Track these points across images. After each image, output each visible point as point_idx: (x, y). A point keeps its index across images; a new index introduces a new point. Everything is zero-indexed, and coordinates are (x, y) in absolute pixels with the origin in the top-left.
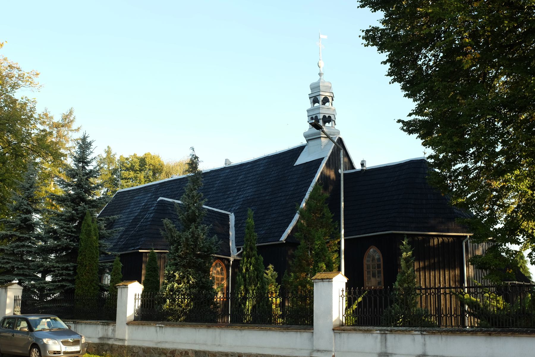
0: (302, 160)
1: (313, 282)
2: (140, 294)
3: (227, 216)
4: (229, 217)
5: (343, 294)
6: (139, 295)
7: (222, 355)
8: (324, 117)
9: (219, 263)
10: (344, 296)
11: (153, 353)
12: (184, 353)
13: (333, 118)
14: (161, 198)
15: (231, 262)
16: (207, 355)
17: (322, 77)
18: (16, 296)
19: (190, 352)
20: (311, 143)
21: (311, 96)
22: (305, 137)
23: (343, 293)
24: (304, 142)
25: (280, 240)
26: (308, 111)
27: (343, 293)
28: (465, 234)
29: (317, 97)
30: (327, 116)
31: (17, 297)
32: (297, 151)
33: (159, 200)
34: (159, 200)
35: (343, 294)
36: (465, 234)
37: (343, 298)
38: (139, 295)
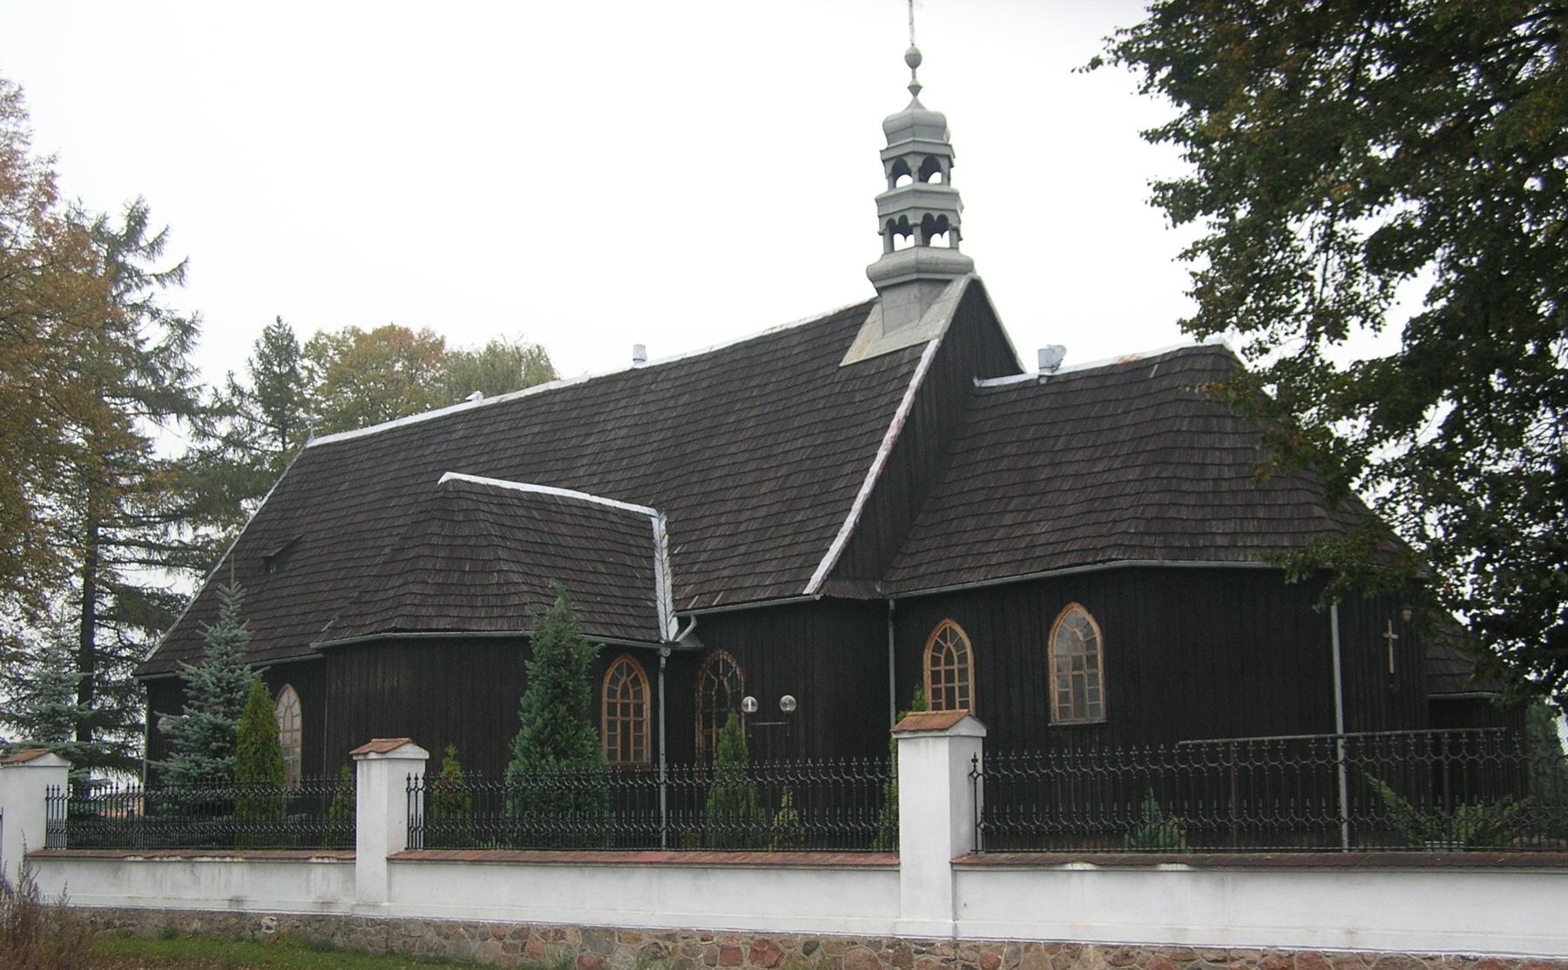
0: (864, 347)
1: (897, 740)
2: (420, 776)
3: (645, 522)
4: (651, 523)
5: (975, 771)
6: (416, 779)
7: (657, 937)
8: (927, 218)
9: (628, 664)
10: (979, 775)
11: (464, 938)
12: (552, 934)
13: (952, 221)
14: (448, 476)
15: (663, 661)
16: (616, 938)
17: (920, 96)
18: (51, 788)
19: (568, 932)
20: (888, 297)
21: (887, 156)
22: (873, 279)
23: (975, 766)
24: (869, 292)
25: (805, 592)
26: (880, 201)
27: (975, 766)
28: (1246, 739)
29: (905, 158)
30: (936, 215)
31: (56, 792)
32: (850, 320)
33: (443, 479)
34: (443, 479)
35: (975, 771)
36: (1246, 739)
37: (975, 779)
38: (416, 779)
